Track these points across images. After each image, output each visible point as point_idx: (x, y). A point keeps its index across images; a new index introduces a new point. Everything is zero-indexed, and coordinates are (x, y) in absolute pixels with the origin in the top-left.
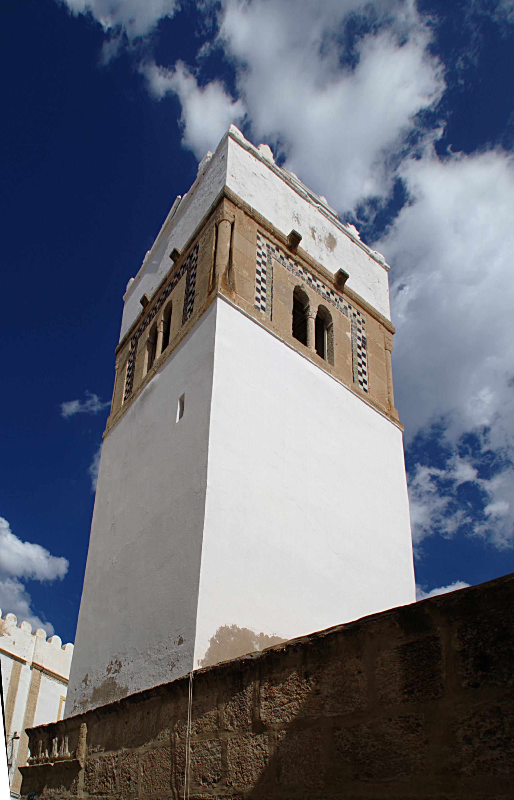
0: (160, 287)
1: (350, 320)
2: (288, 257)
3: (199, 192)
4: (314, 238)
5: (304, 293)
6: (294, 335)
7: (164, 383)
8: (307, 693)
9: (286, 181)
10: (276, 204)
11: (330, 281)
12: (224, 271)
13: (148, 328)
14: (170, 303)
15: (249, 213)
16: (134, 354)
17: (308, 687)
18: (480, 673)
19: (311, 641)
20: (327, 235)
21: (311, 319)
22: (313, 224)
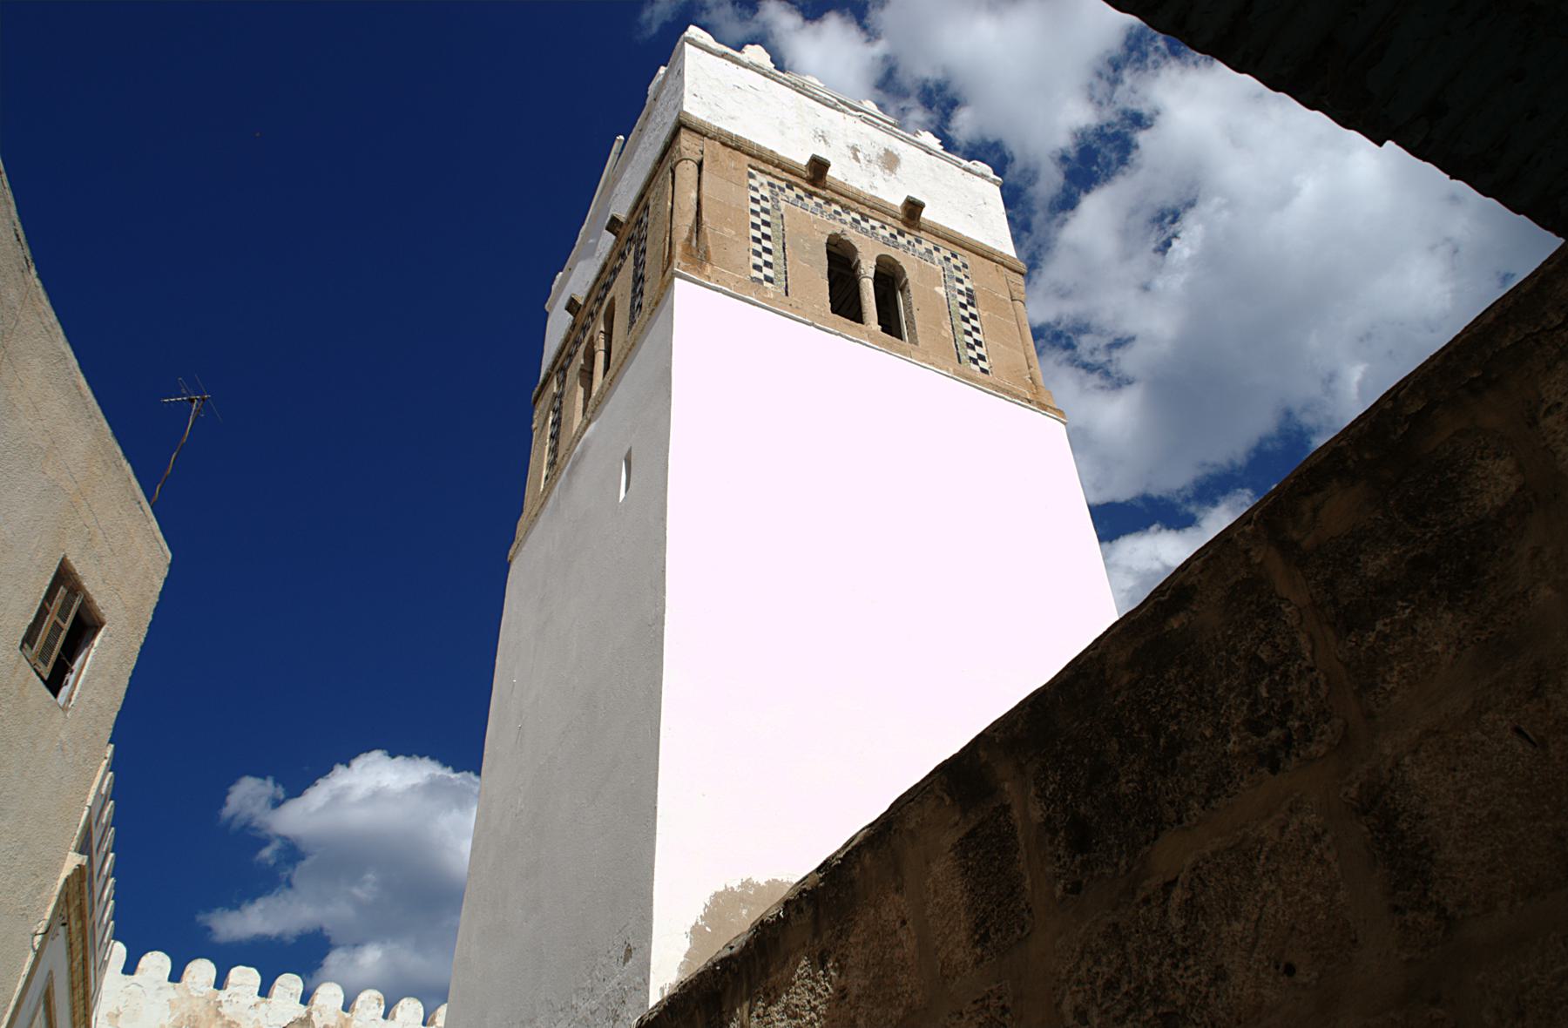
0: (598, 279)
1: (939, 268)
2: (811, 195)
3: (650, 126)
4: (857, 160)
5: (848, 242)
6: (833, 311)
7: (599, 436)
8: (828, 1001)
10: (782, 123)
12: (685, 235)
13: (583, 346)
14: (613, 299)
16: (561, 395)
17: (825, 988)
18: (1079, 858)
19: (822, 879)
20: (882, 153)
22: (851, 141)
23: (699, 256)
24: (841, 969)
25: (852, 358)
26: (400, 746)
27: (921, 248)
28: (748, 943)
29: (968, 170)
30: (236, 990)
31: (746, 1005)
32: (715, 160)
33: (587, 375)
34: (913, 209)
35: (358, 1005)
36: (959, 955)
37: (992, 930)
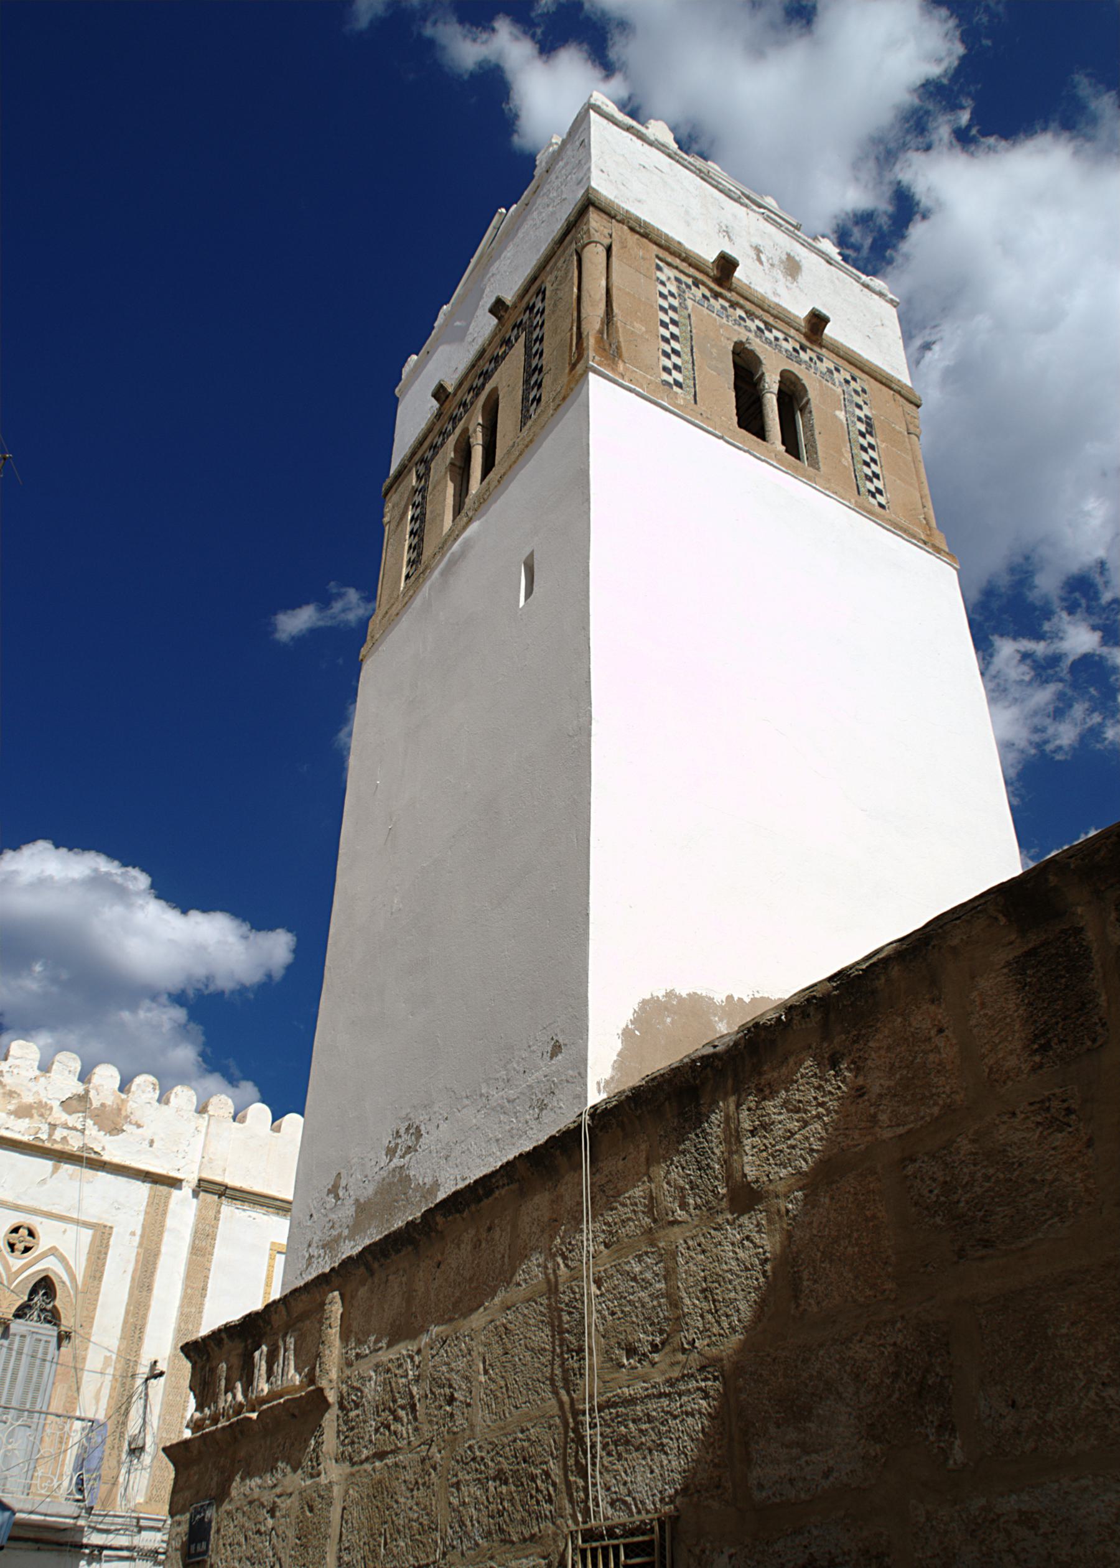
0: (473, 366)
1: (839, 390)
2: (716, 295)
4: (761, 263)
5: (752, 352)
10: (687, 212)
12: (597, 326)
13: (452, 441)
15: (638, 229)
16: (423, 490)
17: (838, 1085)
20: (784, 257)
21: (768, 395)
22: (756, 241)
23: (612, 353)
24: (858, 1070)
25: (747, 477)
26: (70, 837)
27: (823, 366)
28: (736, 1044)
29: (867, 286)
30: (17, 1062)
31: (732, 1100)
32: (624, 247)
33: (461, 471)
34: (817, 322)
35: (134, 1088)
36: (1012, 1062)
37: (1055, 1040)
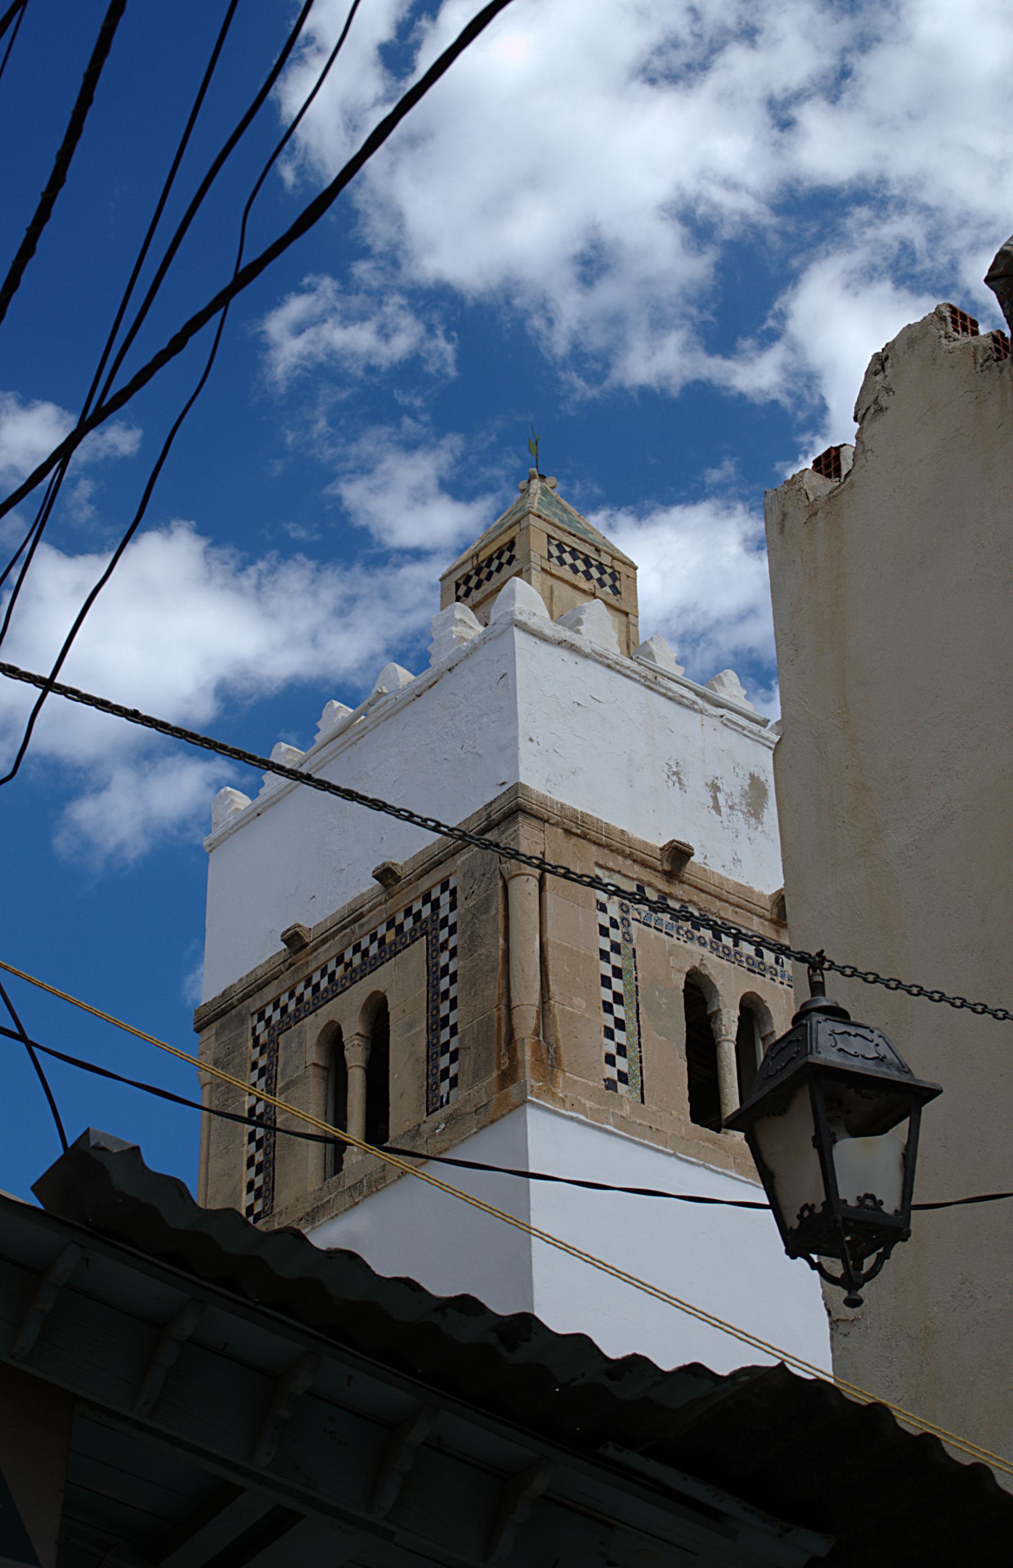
9: (648, 683)
11: (761, 917)
12: (532, 1023)
15: (574, 830)
21: (726, 1045)
